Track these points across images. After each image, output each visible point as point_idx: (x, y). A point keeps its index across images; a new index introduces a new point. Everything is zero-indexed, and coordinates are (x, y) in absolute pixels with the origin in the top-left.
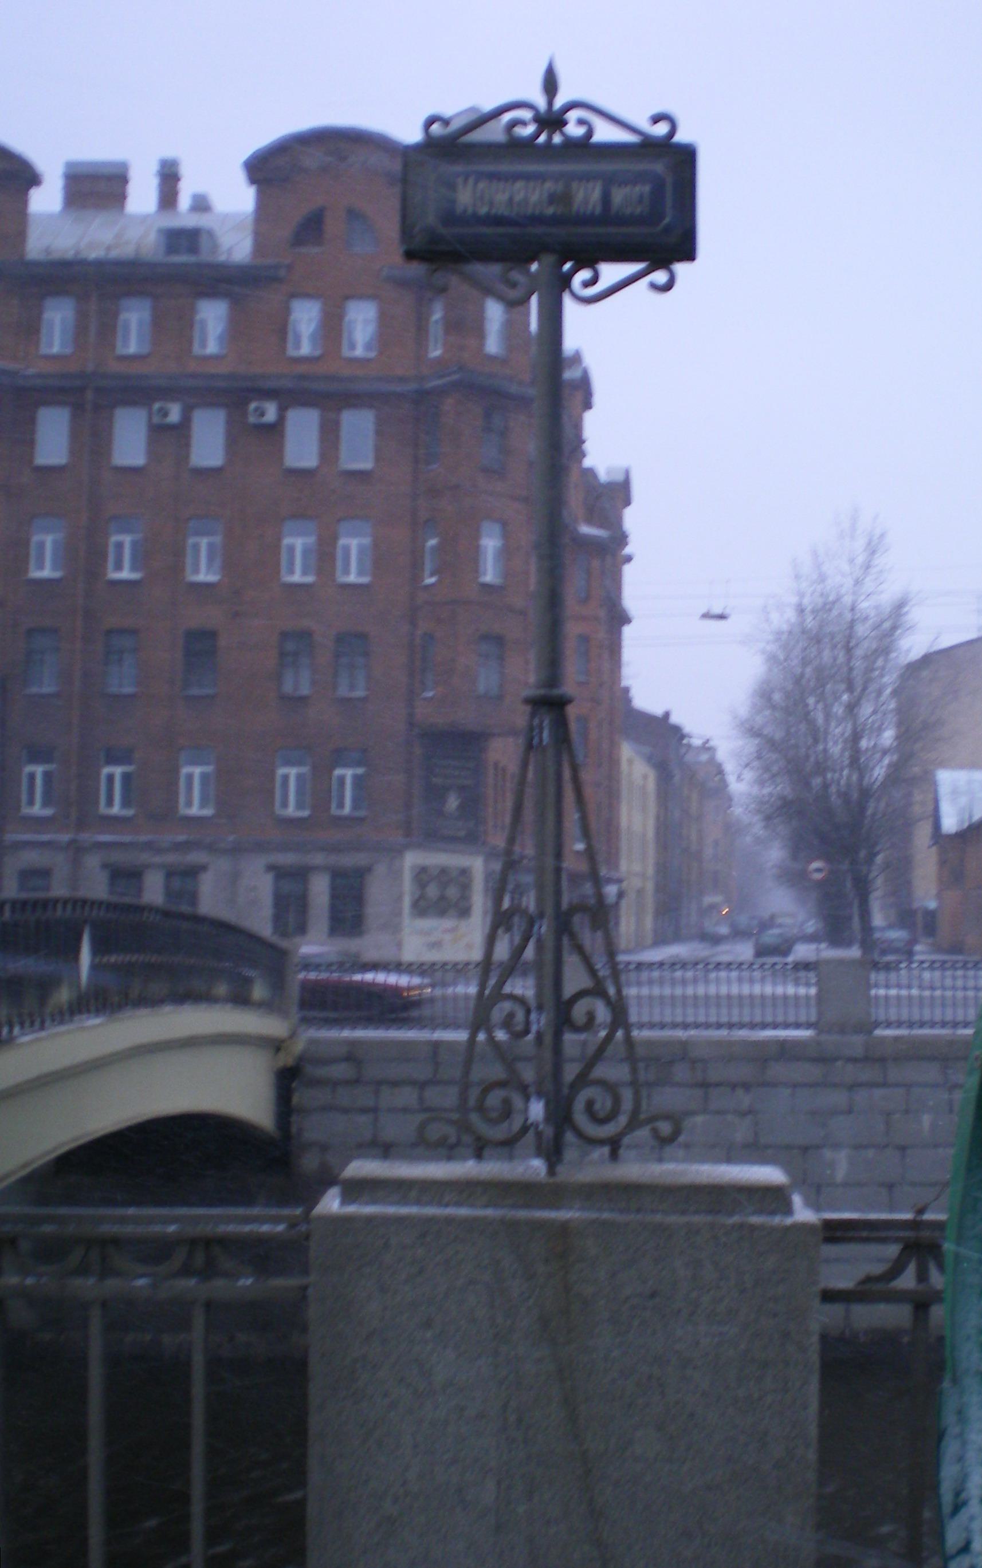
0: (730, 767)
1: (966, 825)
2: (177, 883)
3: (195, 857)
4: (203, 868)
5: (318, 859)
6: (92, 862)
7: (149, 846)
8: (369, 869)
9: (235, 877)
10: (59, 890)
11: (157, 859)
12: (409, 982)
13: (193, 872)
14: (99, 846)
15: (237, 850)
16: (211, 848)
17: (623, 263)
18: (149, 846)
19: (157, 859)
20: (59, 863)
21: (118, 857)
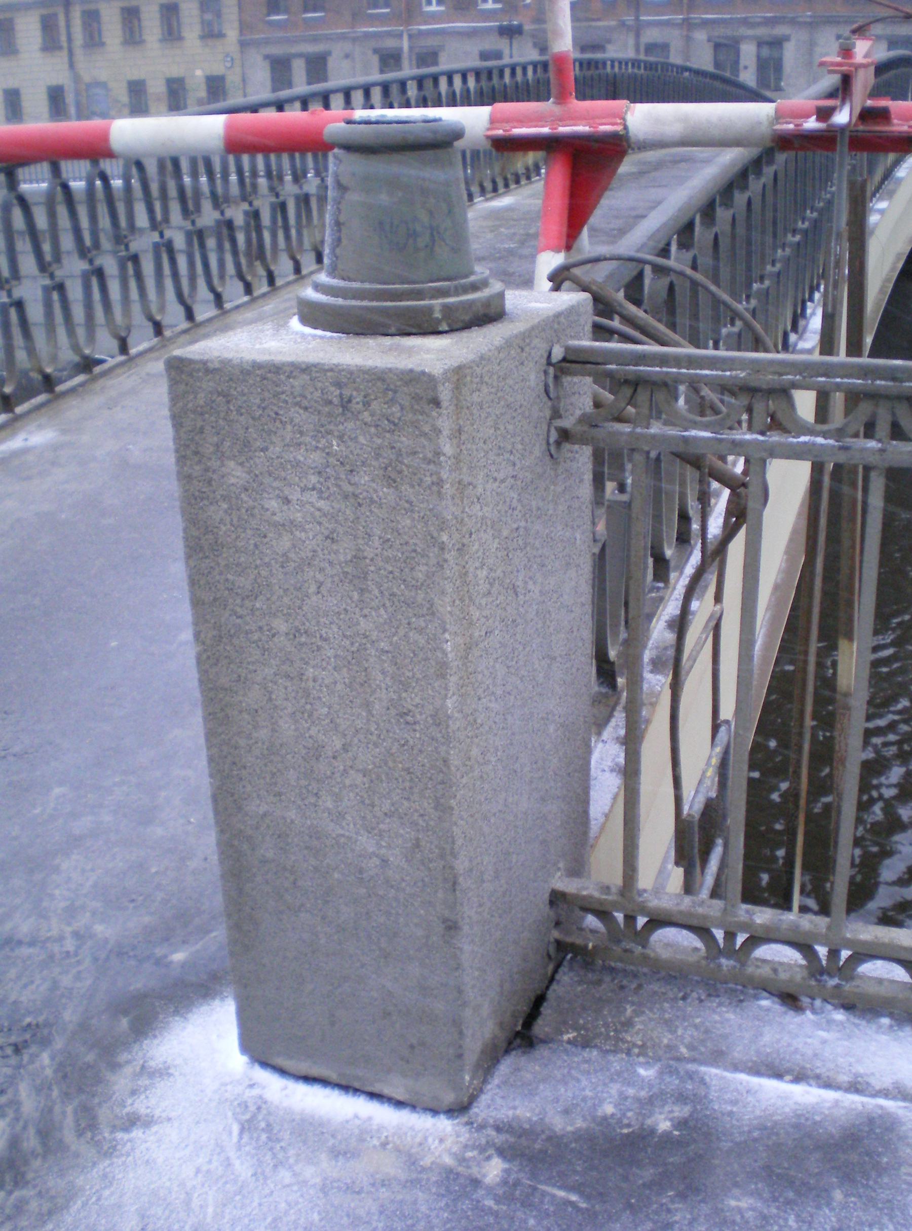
0: (650, 644)
1: (506, 154)
2: (765, 52)
3: (780, 30)
4: (787, 38)
5: (744, 31)
6: (701, 36)
7: (745, 22)
8: (329, 53)
9: (812, 45)
10: (676, 59)
11: (750, 32)
12: (35, 324)
13: (777, 43)
14: (705, 23)
15: (813, 25)
16: (793, 22)
17: (760, 556)
18: (745, 22)
19: (750, 32)
20: (674, 36)
21: (720, 32)
